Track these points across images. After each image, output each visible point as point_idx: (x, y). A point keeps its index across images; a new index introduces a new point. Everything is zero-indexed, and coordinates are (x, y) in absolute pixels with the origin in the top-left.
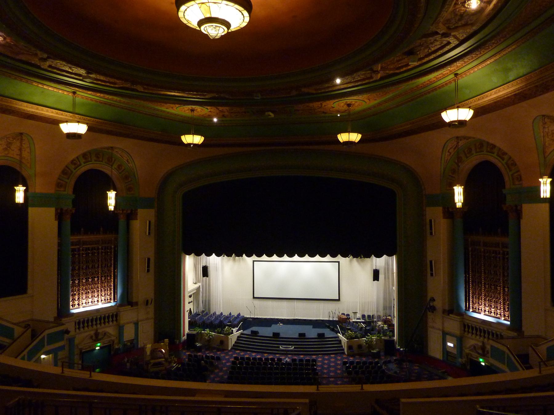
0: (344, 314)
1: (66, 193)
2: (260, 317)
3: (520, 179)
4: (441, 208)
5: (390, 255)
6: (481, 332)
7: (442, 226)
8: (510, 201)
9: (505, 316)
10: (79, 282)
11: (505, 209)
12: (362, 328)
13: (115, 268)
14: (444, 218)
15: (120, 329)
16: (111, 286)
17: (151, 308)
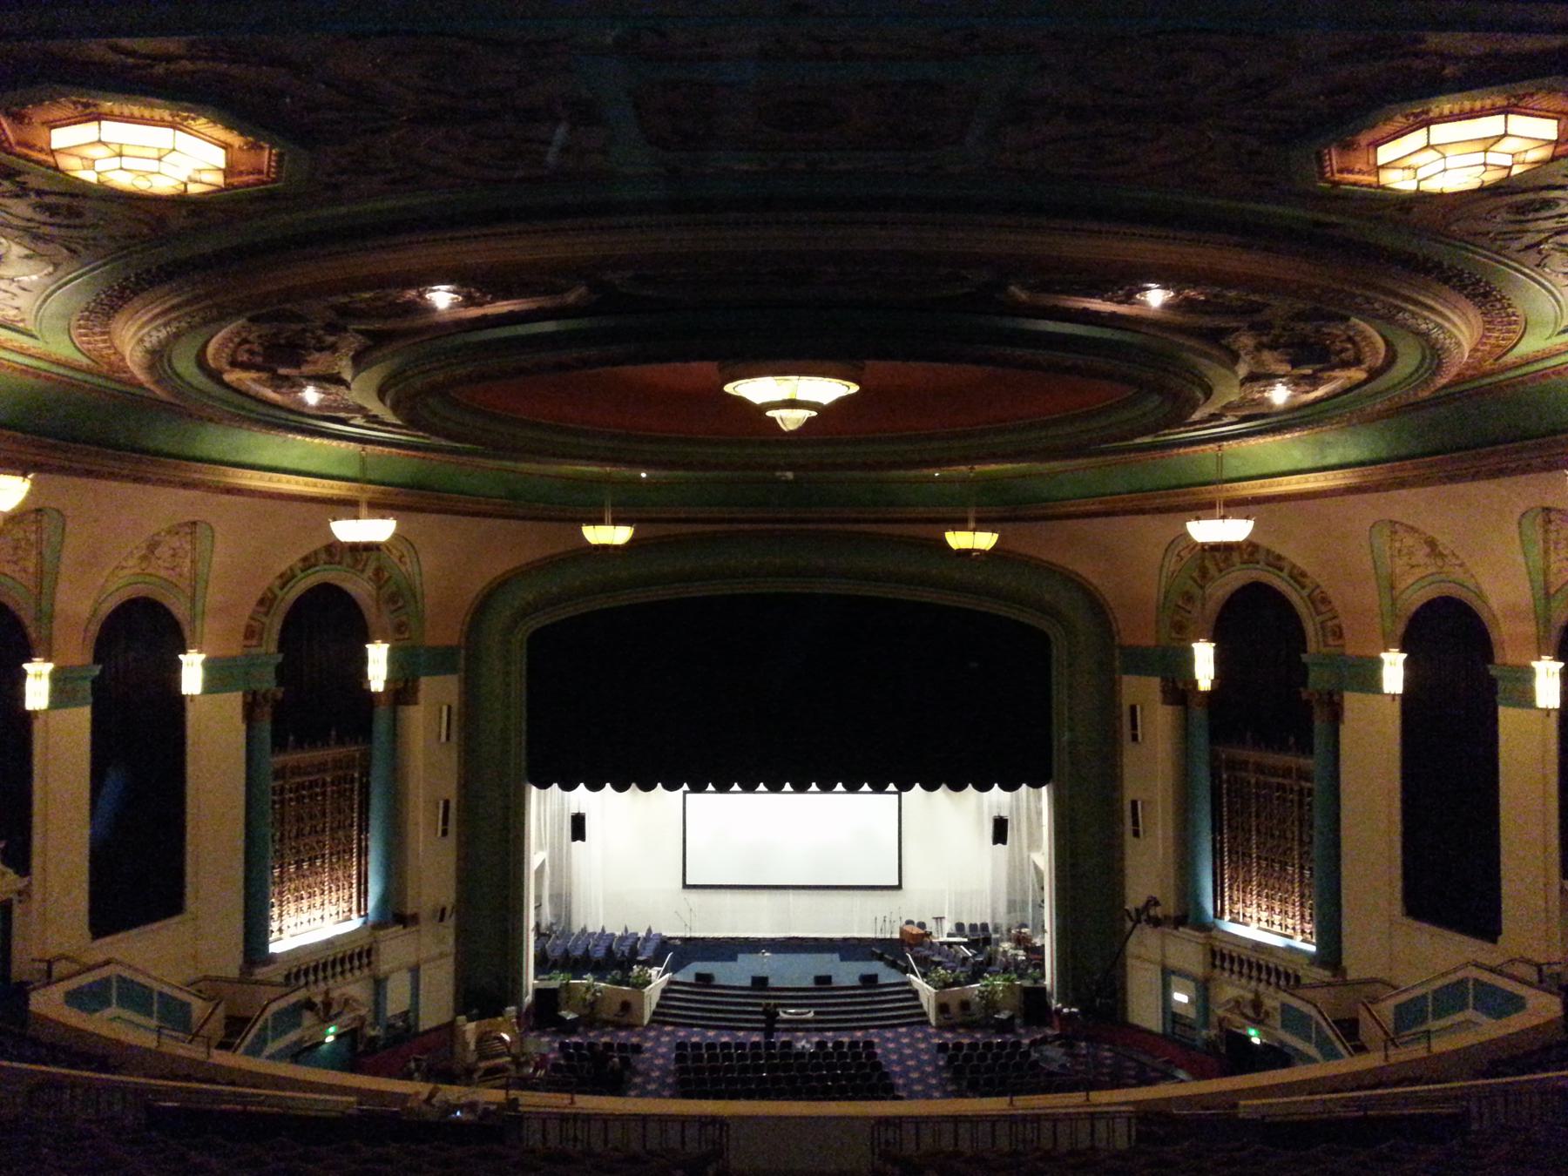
0: (909, 922)
1: (262, 650)
2: (702, 935)
3: (1338, 633)
4: (1157, 680)
5: (1036, 784)
6: (1269, 974)
7: (1159, 721)
8: (1318, 680)
9: (1303, 932)
10: (282, 872)
11: (1304, 696)
12: (966, 959)
13: (364, 828)
14: (1165, 702)
15: (379, 984)
16: (350, 876)
17: (448, 931)
